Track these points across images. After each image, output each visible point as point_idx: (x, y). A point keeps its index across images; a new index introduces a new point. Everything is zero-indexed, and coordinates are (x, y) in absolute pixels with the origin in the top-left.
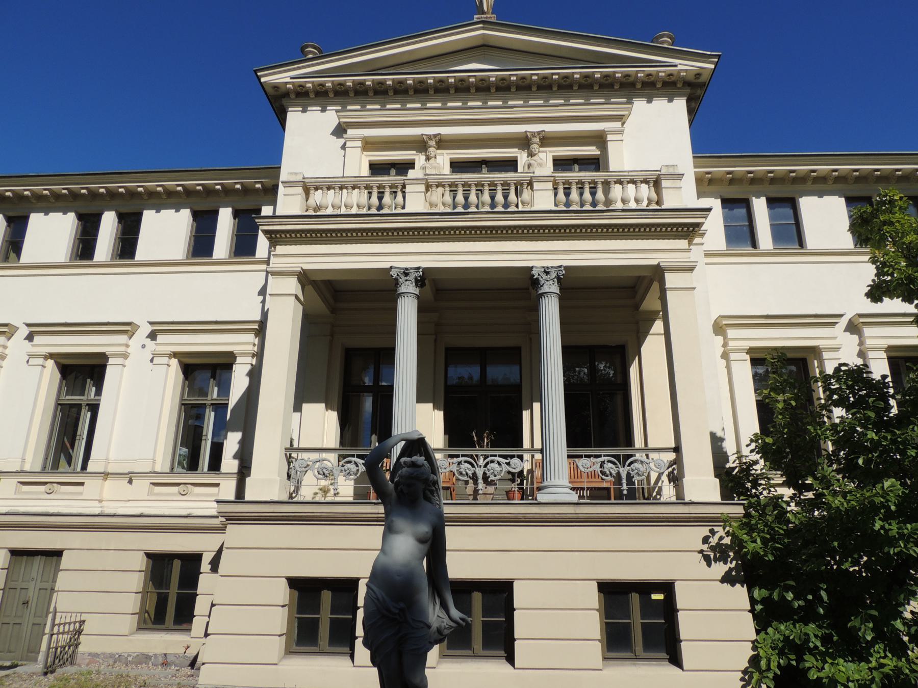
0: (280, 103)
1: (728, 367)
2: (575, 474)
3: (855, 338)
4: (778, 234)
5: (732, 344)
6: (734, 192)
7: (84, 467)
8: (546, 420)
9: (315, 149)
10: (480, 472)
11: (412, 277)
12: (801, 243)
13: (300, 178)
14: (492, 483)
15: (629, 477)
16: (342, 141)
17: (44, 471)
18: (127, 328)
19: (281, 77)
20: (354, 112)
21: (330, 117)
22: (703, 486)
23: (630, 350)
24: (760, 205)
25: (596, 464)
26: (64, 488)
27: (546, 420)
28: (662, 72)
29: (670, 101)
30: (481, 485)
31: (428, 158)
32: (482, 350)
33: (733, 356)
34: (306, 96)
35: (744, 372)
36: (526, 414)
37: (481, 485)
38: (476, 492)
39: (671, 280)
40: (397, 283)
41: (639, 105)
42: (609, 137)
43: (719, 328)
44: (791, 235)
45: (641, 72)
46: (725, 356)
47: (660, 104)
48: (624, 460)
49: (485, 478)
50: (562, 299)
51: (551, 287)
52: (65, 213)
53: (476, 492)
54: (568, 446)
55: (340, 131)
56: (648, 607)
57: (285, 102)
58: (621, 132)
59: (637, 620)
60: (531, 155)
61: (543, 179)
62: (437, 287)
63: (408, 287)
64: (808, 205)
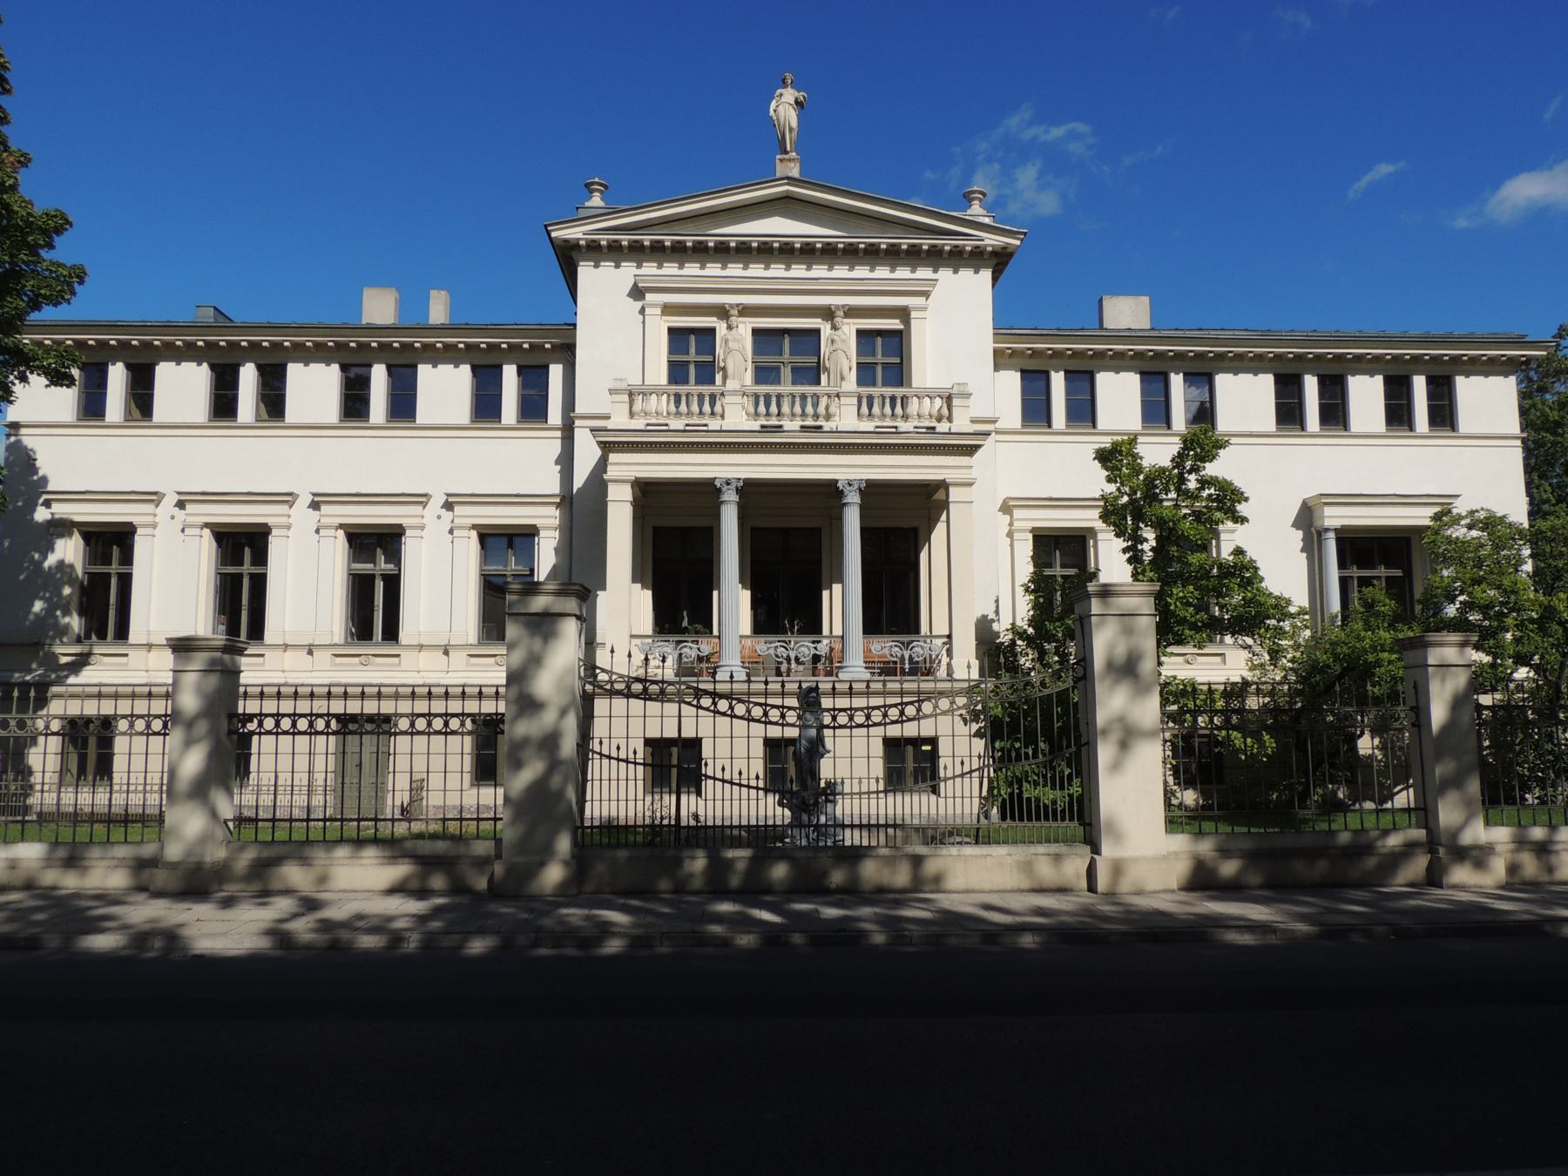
0: (568, 257)
1: (1012, 545)
2: (867, 651)
5: (1017, 524)
6: (1032, 365)
7: (391, 633)
8: (842, 604)
9: (617, 329)
10: (793, 656)
11: (733, 486)
13: (623, 385)
14: (802, 663)
15: (911, 658)
16: (639, 304)
17: (347, 644)
19: (575, 233)
21: (628, 273)
22: (965, 663)
23: (921, 535)
24: (1058, 380)
25: (885, 647)
27: (842, 604)
28: (968, 245)
29: (976, 272)
30: (793, 665)
31: (730, 328)
32: (789, 548)
33: (1016, 536)
34: (595, 251)
35: (1026, 548)
36: (826, 594)
37: (793, 665)
38: (789, 670)
39: (954, 494)
40: (719, 491)
41: (945, 274)
42: (913, 314)
43: (1006, 508)
45: (947, 244)
46: (1010, 535)
47: (966, 274)
48: (907, 645)
49: (797, 659)
50: (862, 508)
51: (853, 498)
52: (328, 365)
53: (789, 670)
54: (865, 632)
55: (637, 293)
56: (919, 756)
57: (574, 255)
58: (924, 309)
59: (910, 765)
60: (834, 328)
61: (849, 394)
62: (751, 491)
63: (730, 500)
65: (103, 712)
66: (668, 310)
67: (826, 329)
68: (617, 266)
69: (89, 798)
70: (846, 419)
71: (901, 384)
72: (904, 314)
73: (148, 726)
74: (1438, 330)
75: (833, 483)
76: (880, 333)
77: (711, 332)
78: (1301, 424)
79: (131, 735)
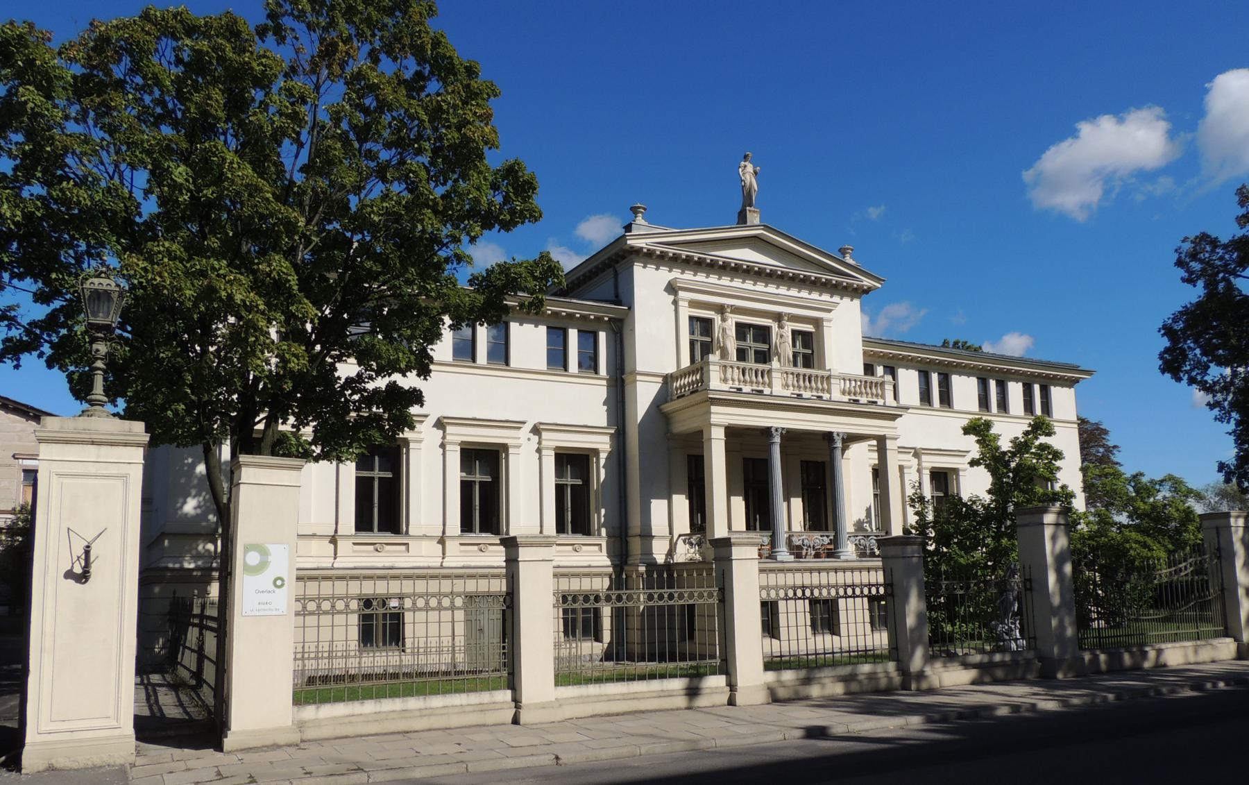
3: (537, 438)
4: (492, 355)
5: (449, 438)
6: (944, 370)
12: (507, 363)
18: (517, 425)
20: (686, 277)
21: (665, 275)
26: (584, 548)
35: (454, 458)
44: (501, 353)
45: (845, 281)
62: (790, 437)
64: (901, 372)
65: (595, 587)
66: (693, 304)
67: (775, 327)
68: (657, 269)
69: (826, 642)
70: (779, 387)
71: (765, 362)
72: (817, 323)
73: (319, 607)
74: (1053, 359)
75: (831, 433)
76: (750, 326)
77: (767, 329)
78: (565, 367)
79: (319, 615)
